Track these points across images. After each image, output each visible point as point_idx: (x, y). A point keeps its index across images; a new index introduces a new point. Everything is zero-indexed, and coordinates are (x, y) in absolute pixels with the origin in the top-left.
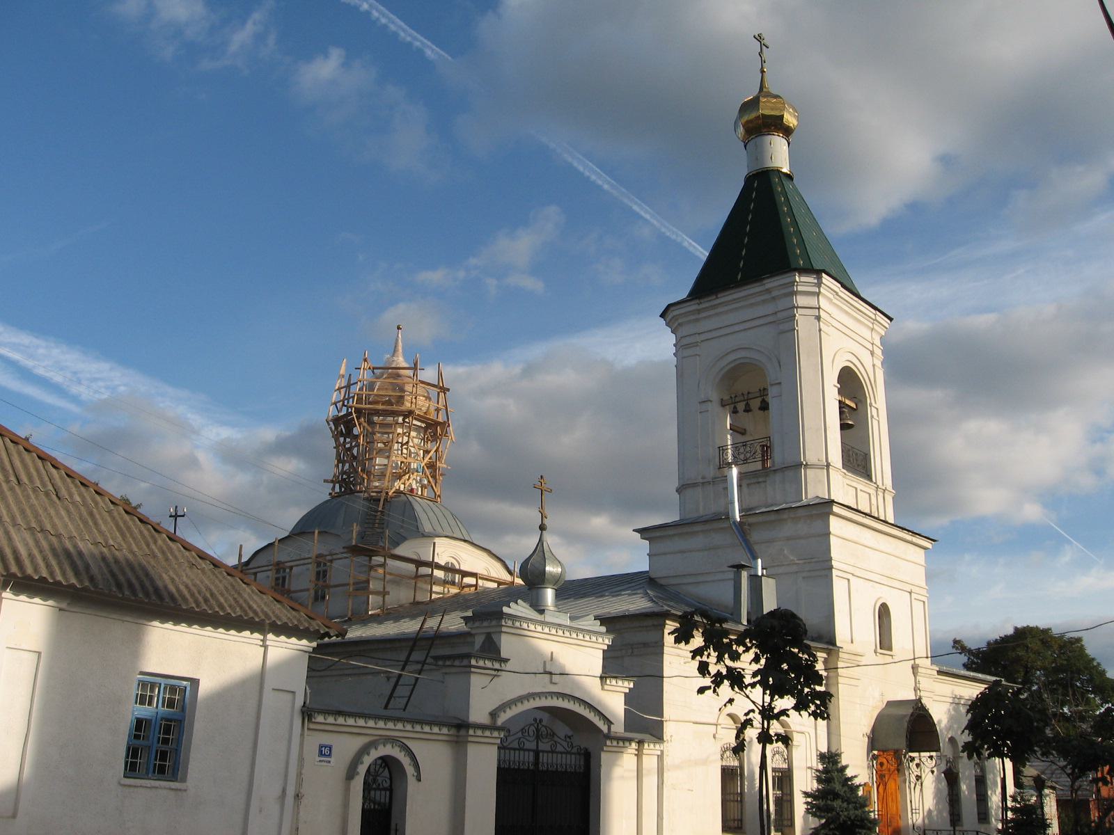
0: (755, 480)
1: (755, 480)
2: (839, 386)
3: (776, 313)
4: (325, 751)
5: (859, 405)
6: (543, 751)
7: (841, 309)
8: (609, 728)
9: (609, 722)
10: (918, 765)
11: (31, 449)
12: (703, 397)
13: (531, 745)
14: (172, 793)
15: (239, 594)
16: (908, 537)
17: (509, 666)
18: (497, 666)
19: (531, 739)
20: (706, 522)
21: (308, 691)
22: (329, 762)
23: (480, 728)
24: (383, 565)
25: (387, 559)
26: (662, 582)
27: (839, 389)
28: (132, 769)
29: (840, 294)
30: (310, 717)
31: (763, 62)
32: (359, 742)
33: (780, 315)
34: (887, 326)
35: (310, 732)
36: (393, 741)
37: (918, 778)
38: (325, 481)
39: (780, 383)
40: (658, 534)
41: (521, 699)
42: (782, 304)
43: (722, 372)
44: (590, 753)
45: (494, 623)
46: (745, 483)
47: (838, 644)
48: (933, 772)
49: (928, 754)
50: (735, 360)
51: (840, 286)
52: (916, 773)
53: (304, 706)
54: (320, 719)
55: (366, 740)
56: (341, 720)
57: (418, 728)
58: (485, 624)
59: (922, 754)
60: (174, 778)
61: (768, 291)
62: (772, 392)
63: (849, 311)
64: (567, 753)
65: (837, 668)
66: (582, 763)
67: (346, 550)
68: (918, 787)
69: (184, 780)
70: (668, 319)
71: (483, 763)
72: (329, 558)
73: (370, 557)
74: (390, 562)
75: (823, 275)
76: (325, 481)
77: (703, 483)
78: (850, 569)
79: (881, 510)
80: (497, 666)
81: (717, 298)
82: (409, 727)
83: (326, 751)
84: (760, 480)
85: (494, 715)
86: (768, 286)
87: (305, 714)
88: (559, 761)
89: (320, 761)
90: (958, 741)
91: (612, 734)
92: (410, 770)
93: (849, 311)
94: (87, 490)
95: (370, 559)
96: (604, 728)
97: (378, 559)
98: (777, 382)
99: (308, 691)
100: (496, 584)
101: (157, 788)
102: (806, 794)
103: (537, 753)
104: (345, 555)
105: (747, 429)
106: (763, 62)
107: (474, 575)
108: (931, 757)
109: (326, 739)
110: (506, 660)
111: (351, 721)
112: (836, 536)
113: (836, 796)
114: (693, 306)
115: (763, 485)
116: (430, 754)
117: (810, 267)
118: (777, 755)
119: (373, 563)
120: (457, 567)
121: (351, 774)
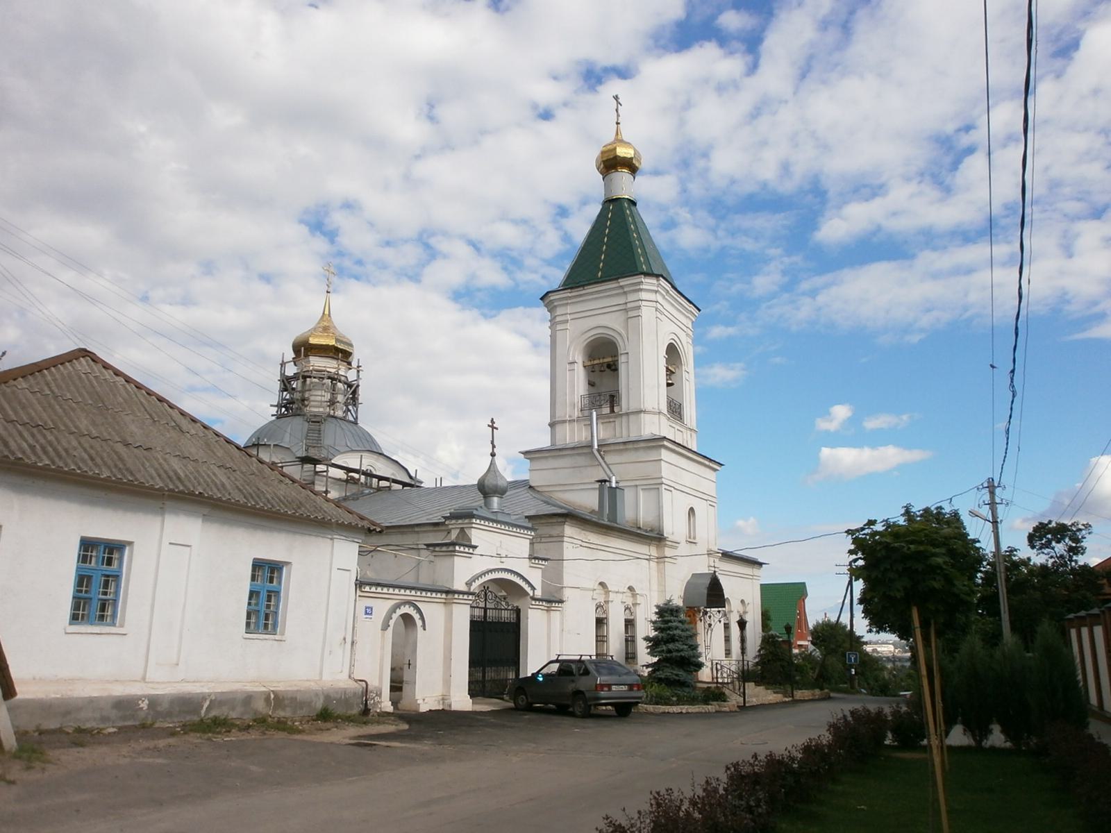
0: (608, 420)
1: (608, 420)
2: (667, 356)
3: (626, 303)
4: (369, 611)
5: (677, 369)
6: (489, 609)
7: (673, 305)
8: (534, 593)
9: (533, 588)
10: (710, 617)
11: (151, 393)
12: (571, 359)
13: (482, 605)
14: (276, 642)
15: (315, 502)
16: (707, 463)
17: (477, 551)
18: (471, 551)
19: (482, 600)
20: (573, 448)
21: (359, 570)
22: (371, 618)
23: (392, 587)
24: (327, 471)
25: (329, 468)
26: (538, 489)
27: (667, 359)
28: (75, 618)
29: (671, 292)
30: (360, 587)
31: (618, 116)
32: (390, 604)
33: (629, 305)
34: (697, 315)
35: (361, 598)
36: (410, 603)
37: (710, 625)
38: (272, 406)
39: (627, 353)
40: (537, 456)
41: (484, 574)
42: (631, 297)
43: (589, 340)
44: (520, 610)
45: (467, 521)
46: (600, 421)
47: (665, 535)
48: (720, 621)
49: (717, 609)
50: (595, 335)
51: (670, 286)
52: (709, 622)
53: (357, 580)
54: (367, 589)
55: (394, 602)
56: (379, 589)
57: (424, 594)
58: (460, 521)
59: (713, 609)
60: (274, 632)
61: (622, 287)
62: (622, 359)
63: (673, 302)
64: (506, 609)
65: (564, 536)
66: (515, 616)
67: (297, 460)
68: (709, 631)
69: (283, 634)
70: (546, 302)
71: (462, 616)
72: (280, 465)
73: (315, 465)
74: (331, 469)
75: (661, 278)
76: (272, 406)
77: (569, 421)
78: (673, 484)
79: (689, 442)
80: (471, 551)
81: (584, 289)
82: (419, 594)
83: (368, 611)
84: (611, 420)
85: (469, 584)
86: (621, 284)
87: (358, 586)
88: (506, 616)
89: (366, 618)
90: (472, 576)
91: (535, 597)
92: (419, 623)
93: (673, 302)
94: (185, 419)
95: (315, 467)
96: (531, 593)
97: (320, 468)
98: (626, 352)
99: (359, 570)
100: (401, 486)
101: (266, 639)
102: (647, 639)
103: (485, 609)
104: (298, 463)
105: (596, 382)
106: (618, 116)
107: (386, 479)
108: (719, 612)
109: (369, 602)
110: (475, 547)
111: (385, 590)
112: (666, 462)
113: (672, 639)
114: (567, 294)
115: (613, 424)
116: (433, 611)
117: (651, 272)
118: (599, 609)
119: (317, 470)
120: (374, 473)
121: (385, 627)
